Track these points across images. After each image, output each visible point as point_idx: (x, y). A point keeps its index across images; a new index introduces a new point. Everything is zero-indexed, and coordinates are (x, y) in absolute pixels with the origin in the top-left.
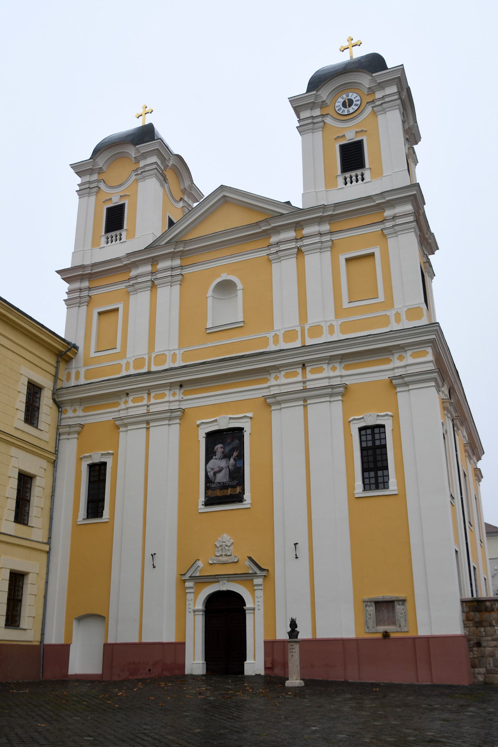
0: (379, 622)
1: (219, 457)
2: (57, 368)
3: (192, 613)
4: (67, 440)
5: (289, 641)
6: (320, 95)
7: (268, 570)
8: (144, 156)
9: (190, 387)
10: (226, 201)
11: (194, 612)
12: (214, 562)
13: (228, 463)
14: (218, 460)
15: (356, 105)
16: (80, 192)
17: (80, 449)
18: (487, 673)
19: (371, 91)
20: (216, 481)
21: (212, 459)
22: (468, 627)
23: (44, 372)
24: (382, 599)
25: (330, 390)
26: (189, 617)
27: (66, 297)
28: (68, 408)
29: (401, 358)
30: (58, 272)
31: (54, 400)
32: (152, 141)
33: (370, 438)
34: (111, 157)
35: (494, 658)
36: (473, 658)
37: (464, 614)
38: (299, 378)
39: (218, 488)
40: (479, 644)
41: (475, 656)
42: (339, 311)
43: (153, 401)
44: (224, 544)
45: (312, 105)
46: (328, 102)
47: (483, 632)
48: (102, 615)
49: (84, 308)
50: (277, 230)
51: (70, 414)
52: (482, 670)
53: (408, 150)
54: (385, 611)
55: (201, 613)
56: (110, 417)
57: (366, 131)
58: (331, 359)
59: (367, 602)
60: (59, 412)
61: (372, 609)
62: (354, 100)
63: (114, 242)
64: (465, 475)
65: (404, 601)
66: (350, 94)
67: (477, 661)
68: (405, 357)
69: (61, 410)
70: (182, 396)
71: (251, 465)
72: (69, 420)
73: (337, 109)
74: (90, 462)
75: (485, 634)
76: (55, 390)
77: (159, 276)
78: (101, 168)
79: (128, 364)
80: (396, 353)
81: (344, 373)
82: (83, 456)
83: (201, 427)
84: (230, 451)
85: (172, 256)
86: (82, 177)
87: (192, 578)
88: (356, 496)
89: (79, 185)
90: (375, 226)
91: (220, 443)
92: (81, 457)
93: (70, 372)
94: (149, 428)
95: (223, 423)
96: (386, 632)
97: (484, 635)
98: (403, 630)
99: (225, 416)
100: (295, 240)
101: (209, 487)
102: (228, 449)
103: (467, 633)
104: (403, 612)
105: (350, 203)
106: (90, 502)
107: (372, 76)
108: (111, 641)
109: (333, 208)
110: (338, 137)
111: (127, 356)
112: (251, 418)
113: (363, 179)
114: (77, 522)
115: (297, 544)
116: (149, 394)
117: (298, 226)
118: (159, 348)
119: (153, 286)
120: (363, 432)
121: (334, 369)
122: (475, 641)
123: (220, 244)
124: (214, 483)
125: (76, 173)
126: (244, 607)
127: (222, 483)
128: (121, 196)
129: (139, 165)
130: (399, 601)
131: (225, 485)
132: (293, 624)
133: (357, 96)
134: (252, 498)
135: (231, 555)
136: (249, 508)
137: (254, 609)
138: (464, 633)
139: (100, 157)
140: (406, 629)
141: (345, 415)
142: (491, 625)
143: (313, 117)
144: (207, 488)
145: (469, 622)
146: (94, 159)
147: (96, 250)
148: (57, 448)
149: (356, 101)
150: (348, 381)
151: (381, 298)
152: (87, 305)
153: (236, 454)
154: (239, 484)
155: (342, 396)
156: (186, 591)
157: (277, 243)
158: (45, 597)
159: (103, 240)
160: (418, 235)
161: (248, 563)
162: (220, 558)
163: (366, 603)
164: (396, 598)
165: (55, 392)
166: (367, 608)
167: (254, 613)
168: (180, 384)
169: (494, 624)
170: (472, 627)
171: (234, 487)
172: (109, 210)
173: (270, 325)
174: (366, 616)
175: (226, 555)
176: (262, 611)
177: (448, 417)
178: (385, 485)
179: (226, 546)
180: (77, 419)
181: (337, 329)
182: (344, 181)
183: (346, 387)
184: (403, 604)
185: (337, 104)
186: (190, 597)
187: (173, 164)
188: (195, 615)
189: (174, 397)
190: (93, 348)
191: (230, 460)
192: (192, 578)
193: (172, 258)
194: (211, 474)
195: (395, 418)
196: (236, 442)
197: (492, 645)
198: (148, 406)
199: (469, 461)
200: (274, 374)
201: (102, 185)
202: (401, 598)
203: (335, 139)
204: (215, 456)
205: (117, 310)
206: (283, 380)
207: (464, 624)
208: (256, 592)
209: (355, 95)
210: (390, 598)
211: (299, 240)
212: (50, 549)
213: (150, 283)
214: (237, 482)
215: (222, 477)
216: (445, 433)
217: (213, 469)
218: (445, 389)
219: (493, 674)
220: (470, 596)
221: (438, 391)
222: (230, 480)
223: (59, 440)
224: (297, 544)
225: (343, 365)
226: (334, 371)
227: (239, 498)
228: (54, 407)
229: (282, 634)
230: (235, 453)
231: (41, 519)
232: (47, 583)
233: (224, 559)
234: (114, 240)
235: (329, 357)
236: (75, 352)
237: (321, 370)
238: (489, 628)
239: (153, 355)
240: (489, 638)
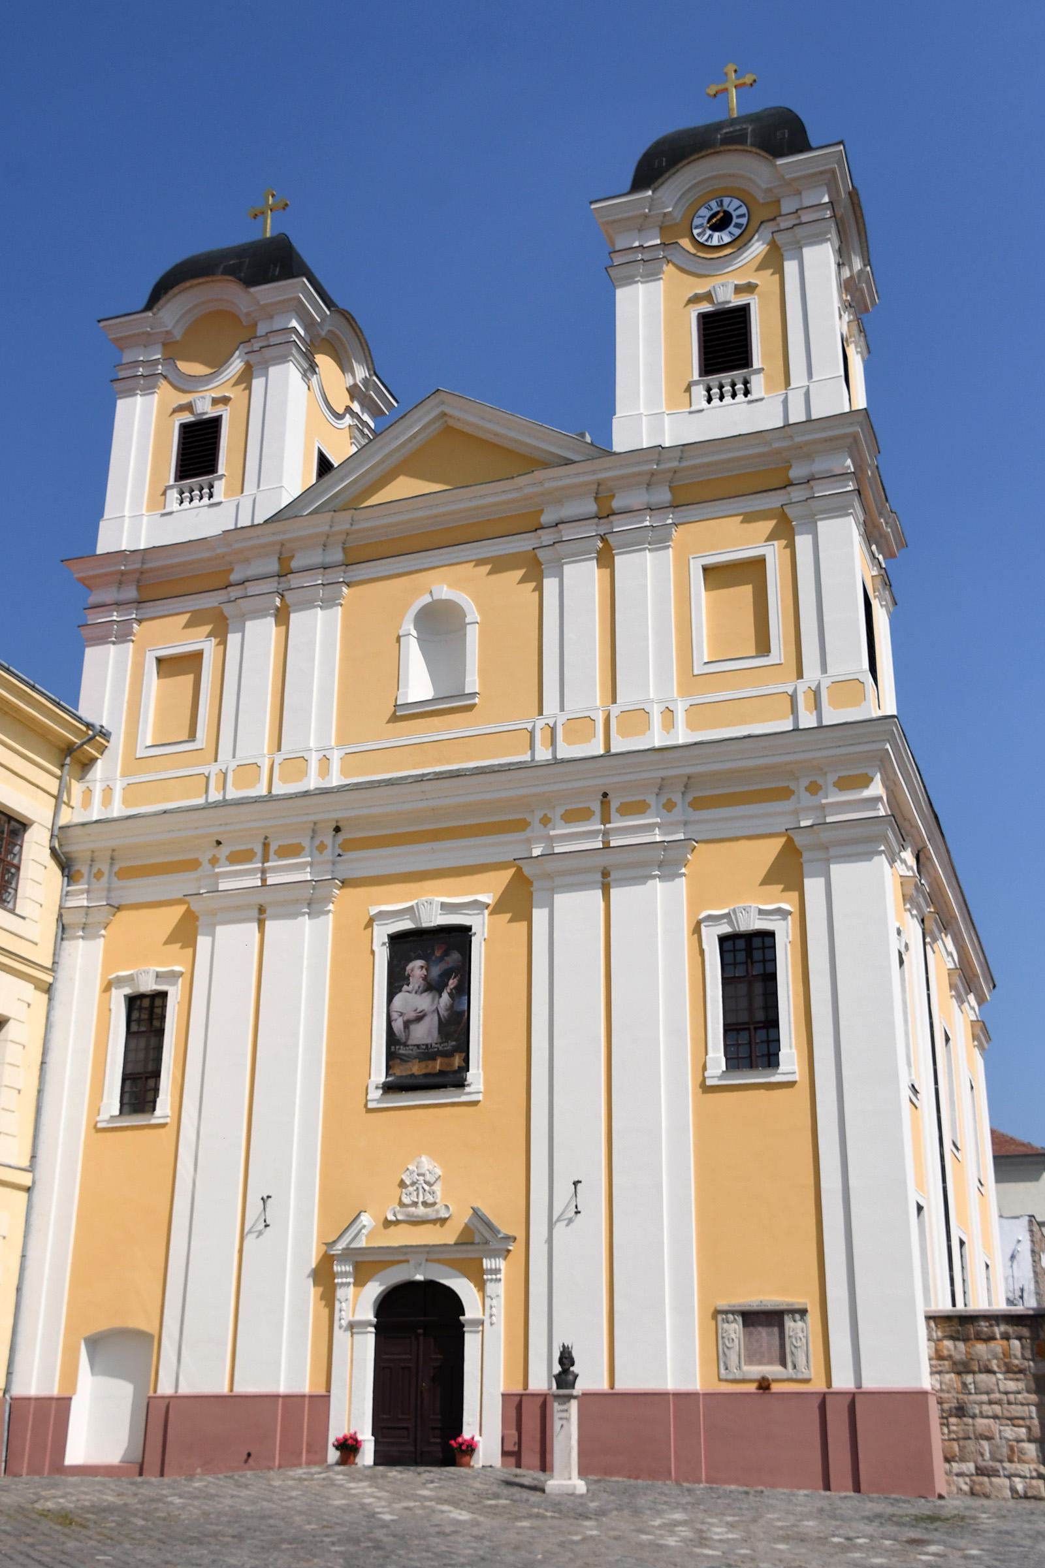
0: (753, 1357)
1: (416, 987)
5: (556, 1393)
13: (436, 1002)
14: (413, 995)
18: (977, 1475)
21: (400, 991)
22: (940, 1373)
24: (757, 1306)
32: (801, 151)
35: (993, 1441)
36: (950, 1440)
37: (933, 1344)
39: (416, 1058)
42: (690, 680)
44: (421, 1178)
47: (970, 1384)
53: (848, 326)
61: (735, 1328)
62: (734, 214)
63: (728, 399)
64: (947, 1039)
68: (823, 787)
69: (69, 872)
73: (695, 232)
75: (975, 1388)
76: (56, 828)
82: (114, 975)
84: (441, 976)
91: (419, 958)
93: (91, 788)
94: (264, 920)
97: (973, 1391)
102: (436, 971)
113: (747, 393)
114: (97, 1122)
115: (580, 1182)
122: (954, 1404)
124: (405, 1045)
126: (461, 1318)
127: (424, 1047)
131: (430, 1050)
132: (566, 1358)
133: (741, 206)
138: (932, 1385)
139: (168, 306)
144: (391, 1056)
145: (941, 1362)
149: (739, 217)
153: (452, 984)
154: (456, 1050)
157: (557, 525)
160: (862, 521)
164: (788, 1305)
171: (448, 1054)
175: (425, 1204)
177: (912, 915)
178: (771, 1060)
179: (426, 1182)
181: (680, 717)
182: (706, 393)
186: (346, 1293)
187: (329, 331)
188: (352, 1334)
191: (441, 996)
194: (398, 1025)
196: (455, 957)
199: (959, 1007)
202: (797, 1307)
204: (408, 985)
210: (775, 1305)
212: (34, 1182)
214: (454, 1043)
215: (424, 1033)
216: (903, 950)
217: (402, 1014)
218: (908, 856)
220: (949, 1306)
221: (892, 862)
222: (440, 1041)
224: (580, 1182)
229: (540, 1381)
230: (451, 981)
232: (23, 1256)
233: (421, 1210)
236: (102, 744)
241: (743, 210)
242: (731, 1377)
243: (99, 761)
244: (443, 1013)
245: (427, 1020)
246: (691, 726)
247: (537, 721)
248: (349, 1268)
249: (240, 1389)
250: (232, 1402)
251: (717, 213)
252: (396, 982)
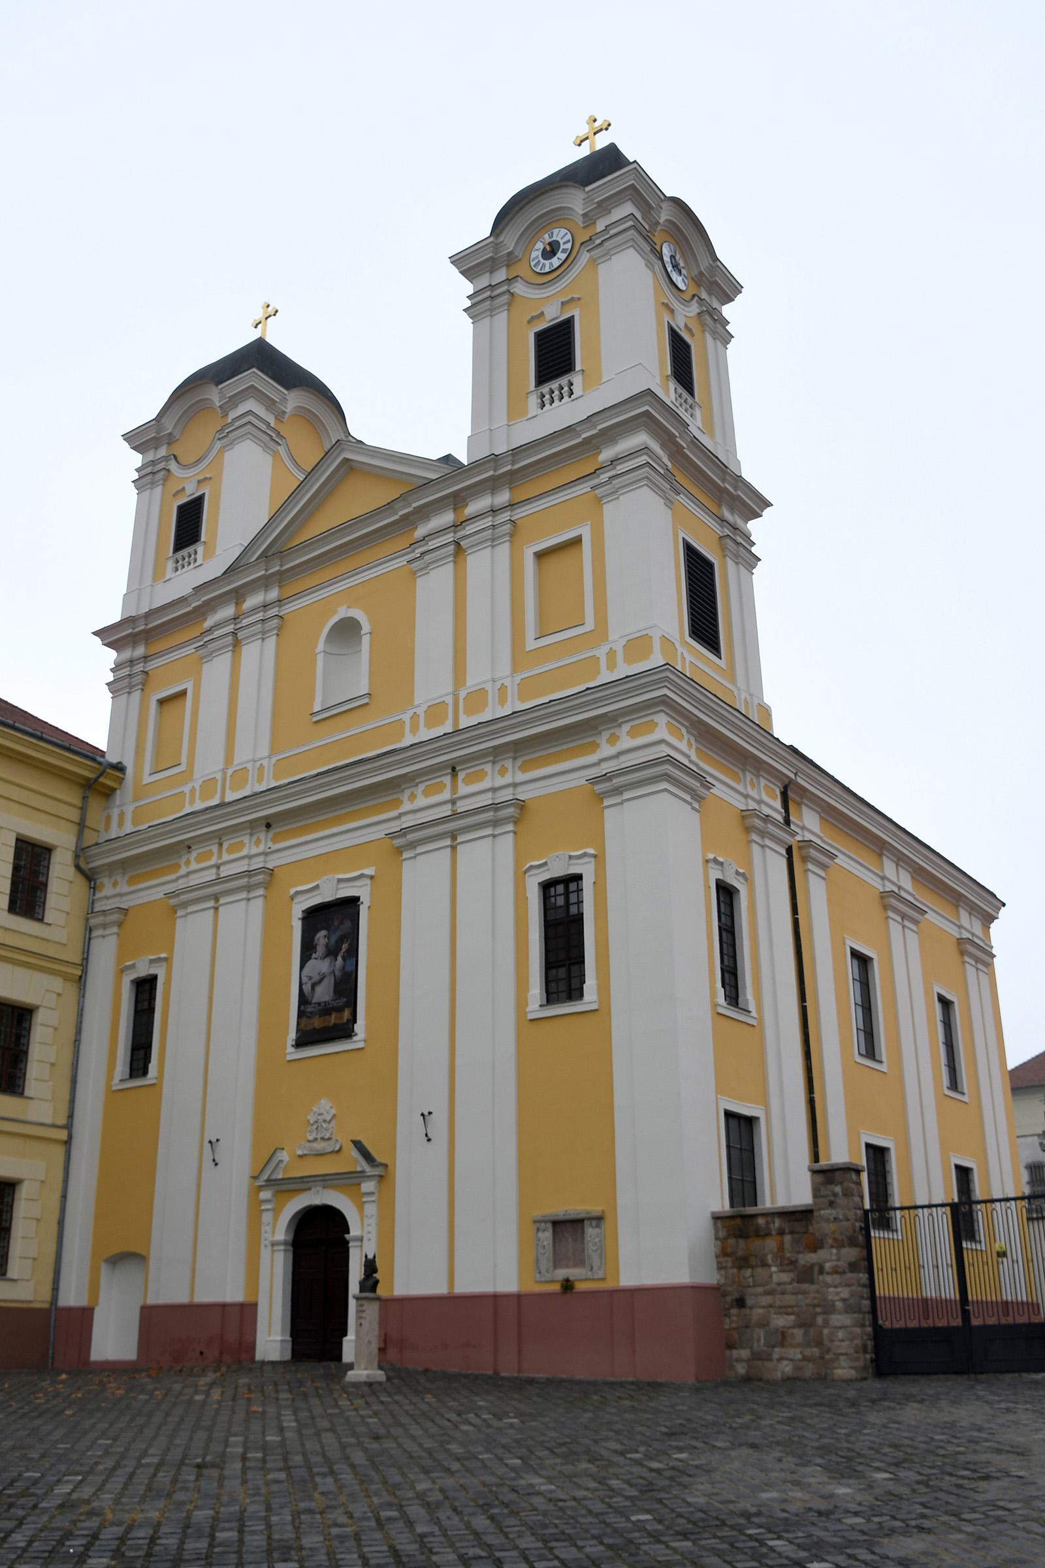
0: (557, 1263)
2: (83, 809)
3: (269, 1247)
4: (100, 939)
7: (386, 1166)
8: (604, 207)
9: (332, 811)
10: (352, 469)
12: (305, 1152)
15: (564, 251)
16: (472, 310)
17: (121, 955)
19: (589, 219)
20: (314, 1001)
22: (725, 1268)
25: (491, 813)
26: (265, 1254)
28: (105, 881)
30: (95, 633)
31: (77, 867)
34: (185, 412)
36: (730, 1329)
37: (719, 1243)
38: (446, 795)
40: (740, 1303)
41: (734, 1325)
42: (519, 658)
43: (463, 789)
45: (490, 263)
48: (138, 1252)
49: (504, 550)
50: (424, 513)
52: (744, 1353)
54: (570, 1240)
55: (282, 1247)
56: (158, 894)
57: (579, 299)
58: (496, 754)
59: (540, 1222)
61: (547, 1236)
63: (556, 403)
65: (599, 1219)
66: (556, 231)
67: (736, 1336)
69: (95, 884)
70: (270, 844)
71: (368, 968)
72: (105, 902)
73: (533, 264)
74: (134, 976)
75: (754, 1281)
77: (245, 622)
78: (170, 434)
79: (611, 654)
81: (521, 777)
82: (528, 865)
83: (296, 900)
84: (337, 942)
85: (265, 583)
86: (474, 281)
87: (270, 1182)
88: (531, 1016)
89: (138, 470)
90: (582, 483)
95: (327, 894)
96: (567, 1280)
98: (596, 1277)
99: (330, 876)
100: (453, 528)
101: (303, 1011)
102: (334, 939)
103: (723, 1281)
104: (597, 1240)
105: (540, 444)
106: (550, 965)
108: (151, 1301)
109: (510, 458)
110: (533, 318)
111: (610, 638)
112: (372, 877)
113: (571, 393)
116: (221, 845)
117: (458, 500)
118: (242, 756)
119: (236, 644)
121: (503, 772)
122: (736, 1296)
123: (336, 553)
125: (463, 273)
126: (347, 1236)
128: (199, 482)
129: (595, 228)
130: (591, 1219)
134: (368, 1028)
135: (329, 1139)
136: (363, 1048)
137: (361, 1239)
140: (600, 1274)
142: (765, 1265)
144: (301, 1014)
147: (160, 586)
149: (564, 243)
150: (524, 794)
151: (590, 625)
152: (142, 690)
154: (347, 1005)
155: (516, 823)
158: (61, 1223)
159: (534, 400)
161: (355, 1153)
162: (315, 1145)
165: (80, 853)
166: (540, 1234)
167: (361, 1246)
168: (264, 822)
169: (770, 1261)
170: (732, 1268)
171: (340, 1010)
172: (541, 337)
173: (407, 697)
174: (537, 1251)
175: (322, 1139)
179: (325, 1121)
180: (118, 899)
183: (521, 805)
184: (598, 1226)
185: (534, 254)
186: (267, 1217)
188: (273, 1251)
190: (147, 769)
192: (270, 1182)
193: (493, 490)
194: (307, 988)
196: (348, 924)
197: (764, 1304)
198: (218, 867)
201: (173, 466)
202: (593, 1214)
203: (529, 322)
205: (577, 541)
206: (626, 742)
207: (718, 1263)
208: (367, 1206)
209: (564, 231)
211: (459, 528)
213: (230, 639)
215: (324, 994)
217: (310, 978)
219: (762, 1359)
225: (519, 762)
227: (345, 1032)
228: (80, 881)
231: (50, 1083)
233: (319, 1146)
234: (556, 399)
235: (491, 750)
237: (480, 776)
238: (759, 1270)
239: (463, 694)
240: (760, 1290)
242: (543, 1279)
243: (118, 791)
244: (338, 973)
245: (325, 981)
249: (461, 1288)
250: (452, 1300)
252: (308, 949)
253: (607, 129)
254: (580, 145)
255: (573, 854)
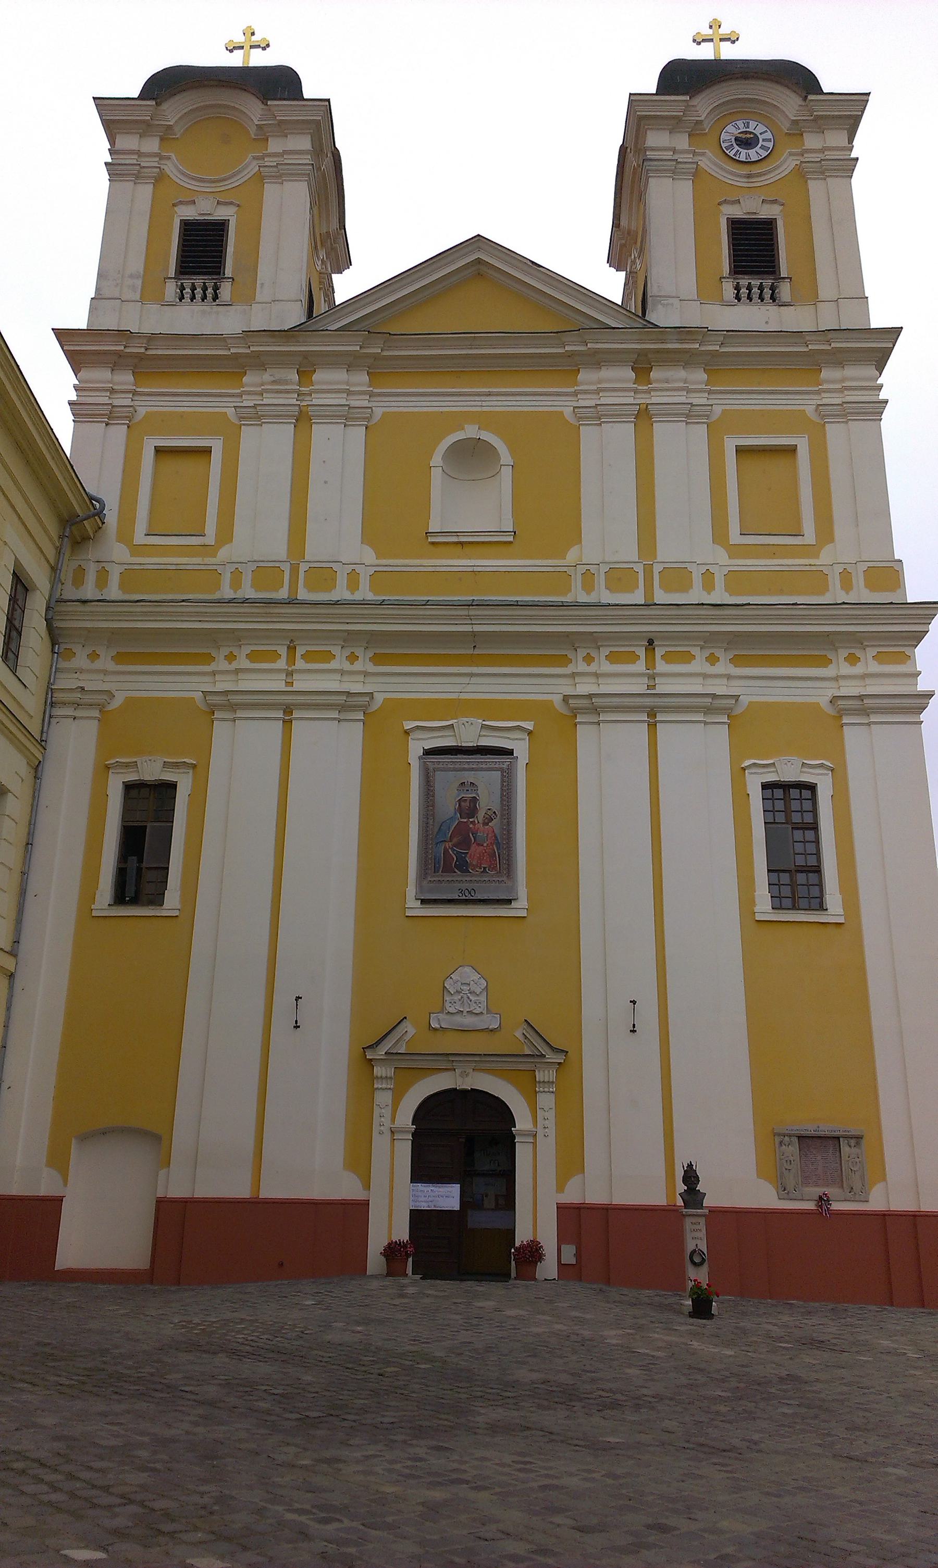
6: (164, 110)
11: (392, 1132)
23: (39, 553)
26: (381, 1143)
27: (73, 396)
28: (77, 649)
29: (852, 660)
32: (294, 99)
33: (795, 805)
46: (707, 127)
51: (81, 660)
60: (53, 652)
61: (792, 1150)
66: (752, 124)
68: (216, 659)
73: (724, 145)
74: (132, 777)
78: (169, 127)
80: (842, 647)
83: (412, 736)
88: (759, 917)
92: (106, 763)
107: (805, 98)
108: (177, 1190)
112: (530, 733)
113: (215, 298)
120: (134, 793)
133: (766, 131)
141: (737, 753)
143: (139, 153)
146: (158, 100)
148: (45, 734)
156: (376, 1086)
162: (458, 1019)
163: (781, 1137)
167: (534, 1144)
176: (552, 1140)
178: (157, 899)
186: (383, 1098)
189: (230, 664)
195: (839, 773)
198: (290, 674)
200: (304, 647)
223: (51, 717)
226: (713, 665)
239: (303, 567)
241: (769, 135)
246: (255, 586)
247: (301, 564)
248: (390, 1072)
251: (751, 133)
253: (264, 49)
254: (231, 51)
255: (805, 762)
